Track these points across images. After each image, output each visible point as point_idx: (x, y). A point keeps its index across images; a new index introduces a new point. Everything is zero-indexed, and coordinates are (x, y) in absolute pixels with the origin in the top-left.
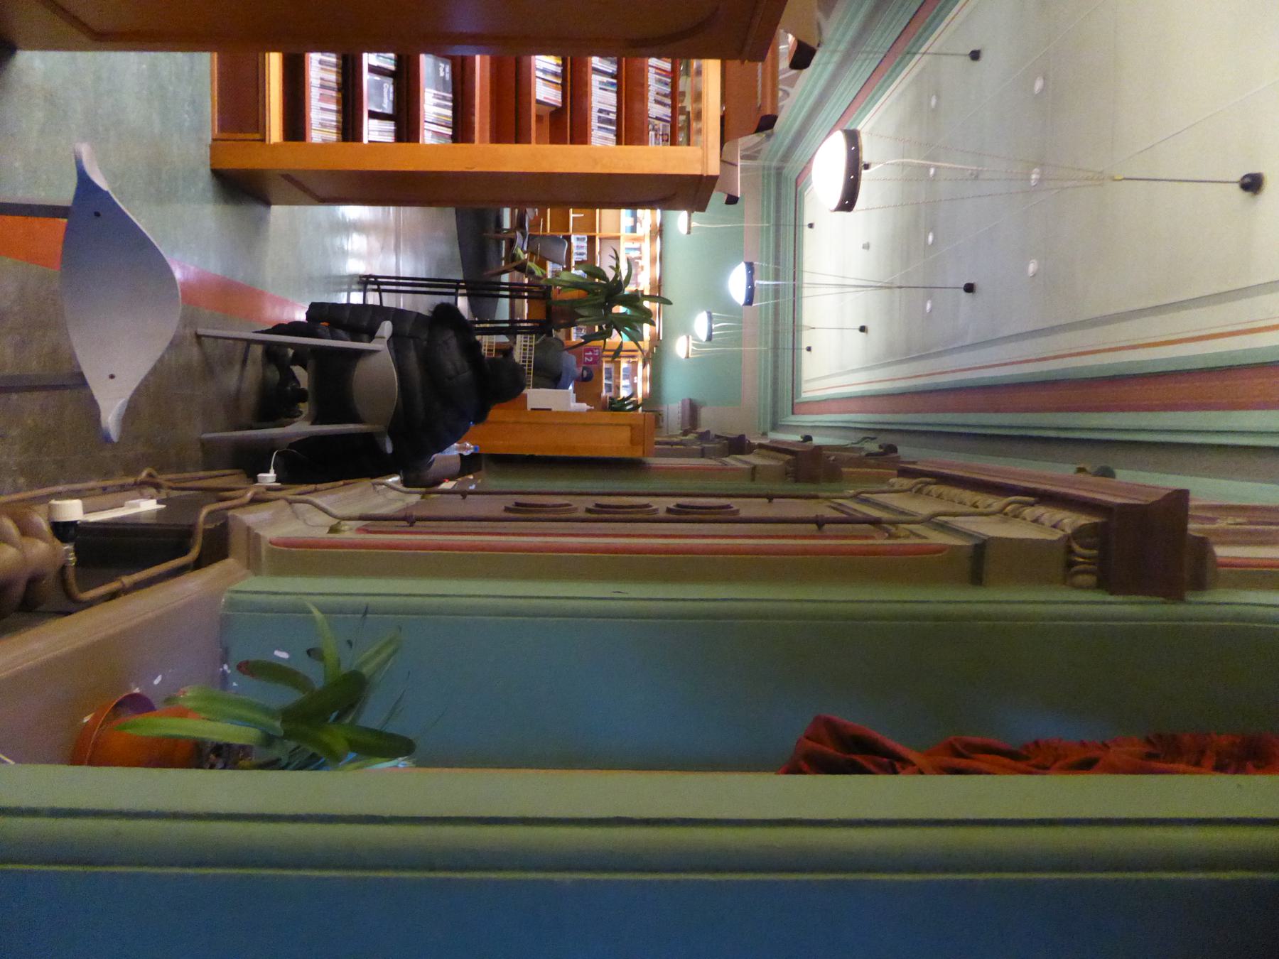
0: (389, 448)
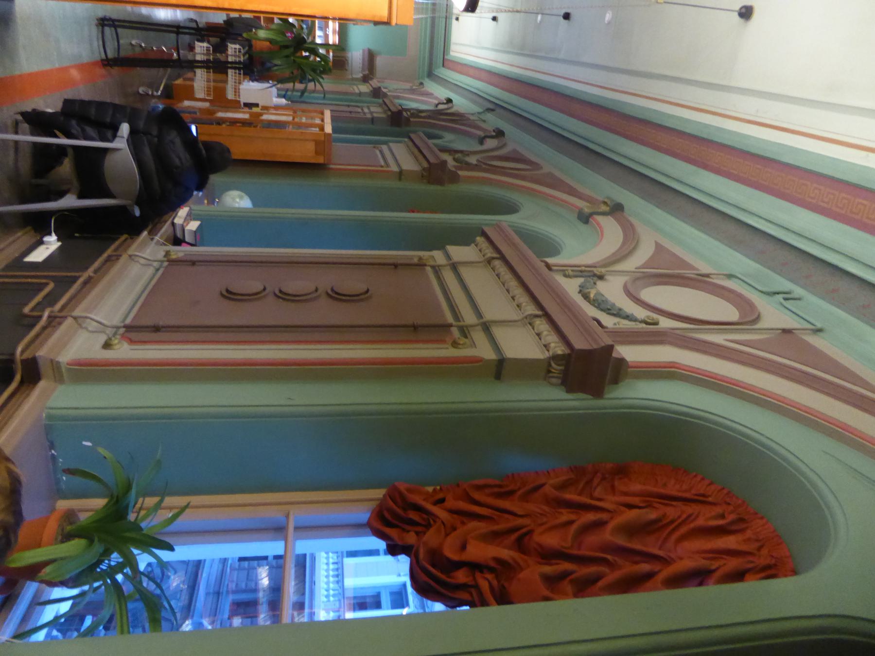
0: (137, 213)
